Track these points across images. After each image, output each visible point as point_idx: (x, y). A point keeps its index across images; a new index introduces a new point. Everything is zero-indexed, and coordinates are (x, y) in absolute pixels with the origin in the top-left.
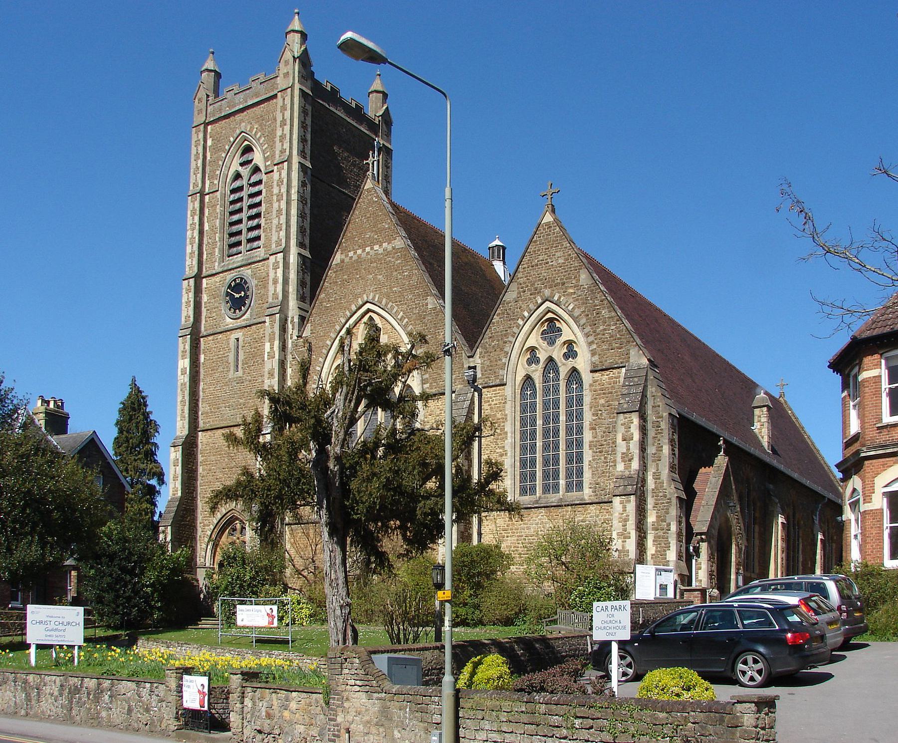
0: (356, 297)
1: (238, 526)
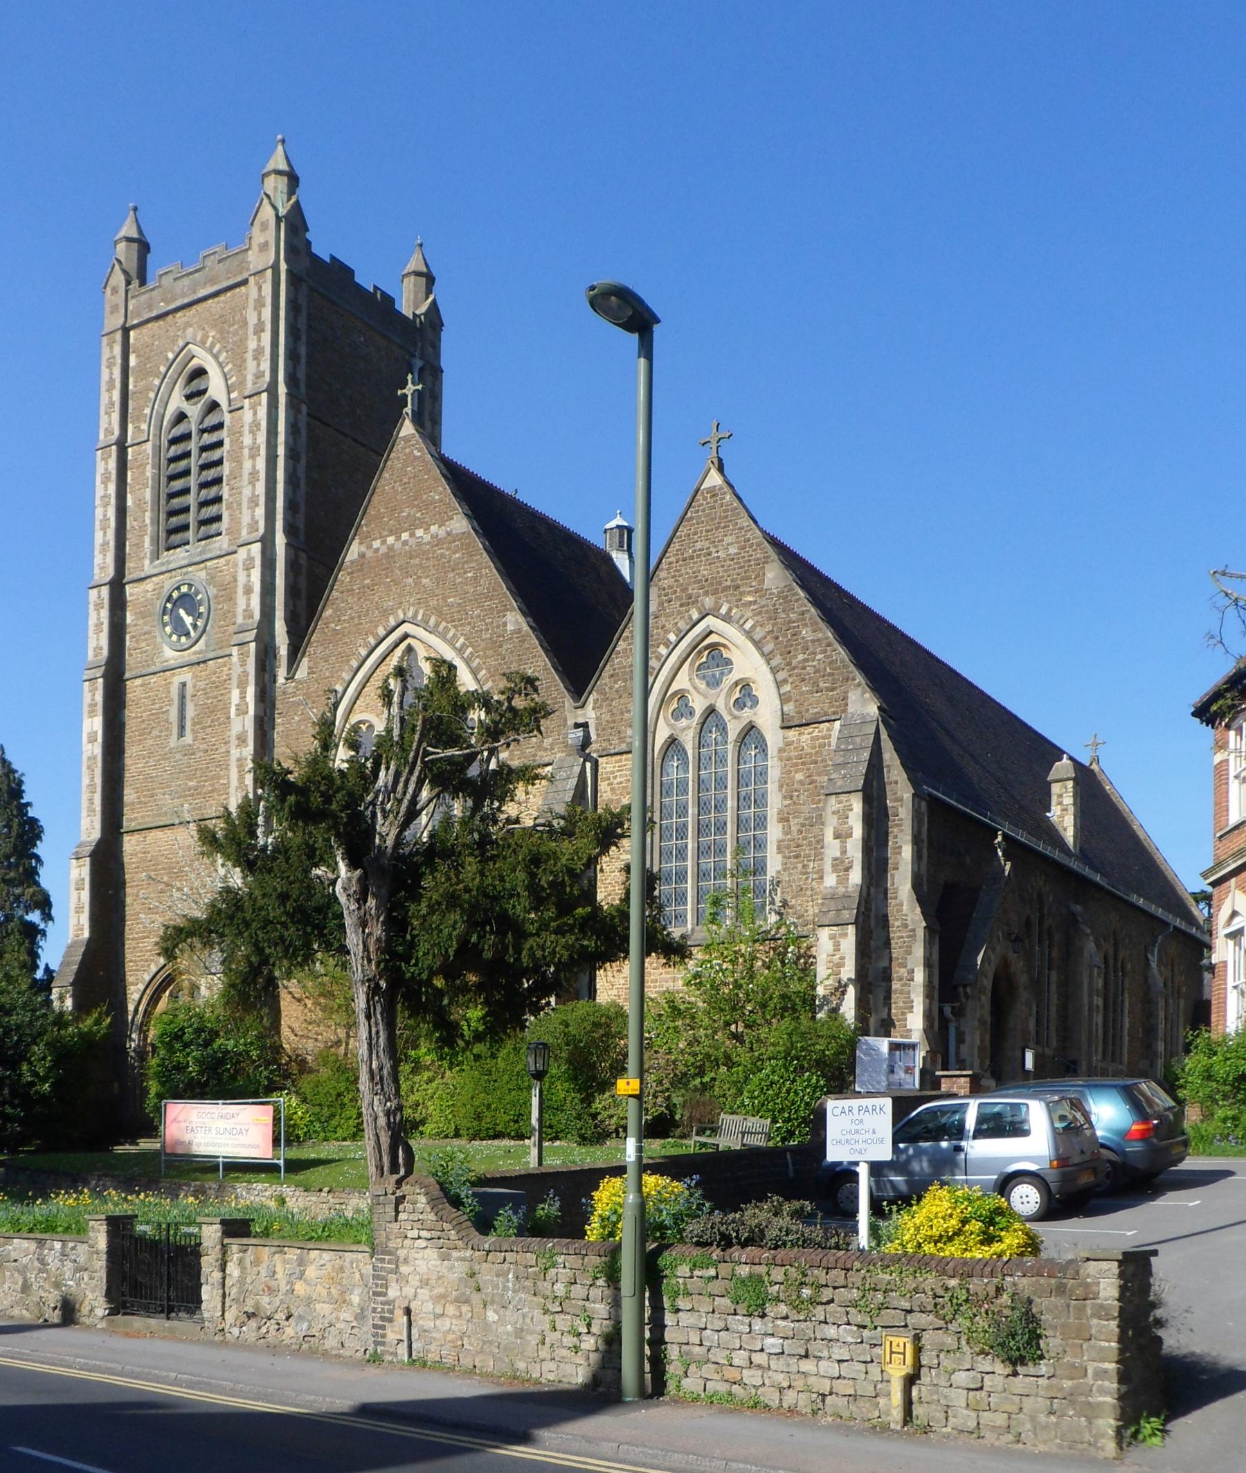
0: (386, 613)
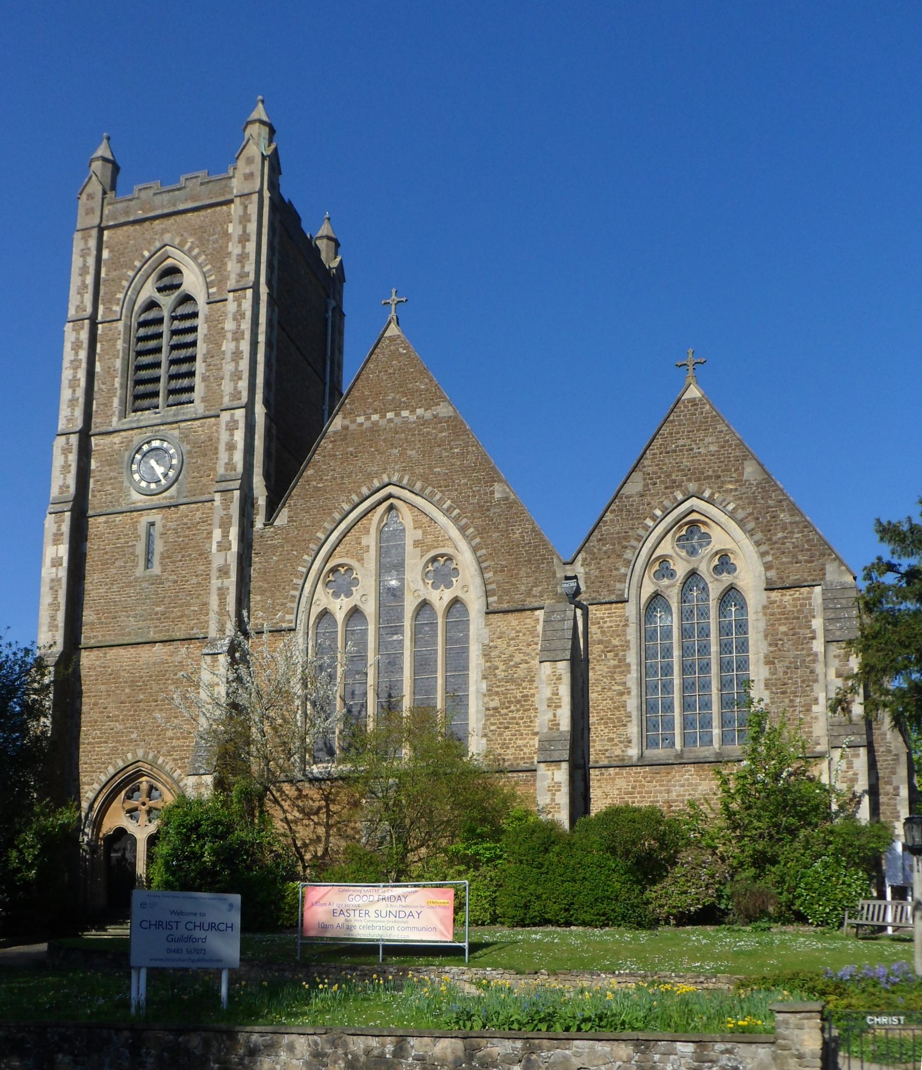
0: (370, 476)
1: (144, 786)
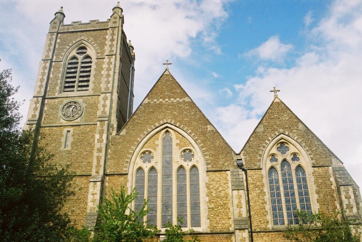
0: (159, 120)
